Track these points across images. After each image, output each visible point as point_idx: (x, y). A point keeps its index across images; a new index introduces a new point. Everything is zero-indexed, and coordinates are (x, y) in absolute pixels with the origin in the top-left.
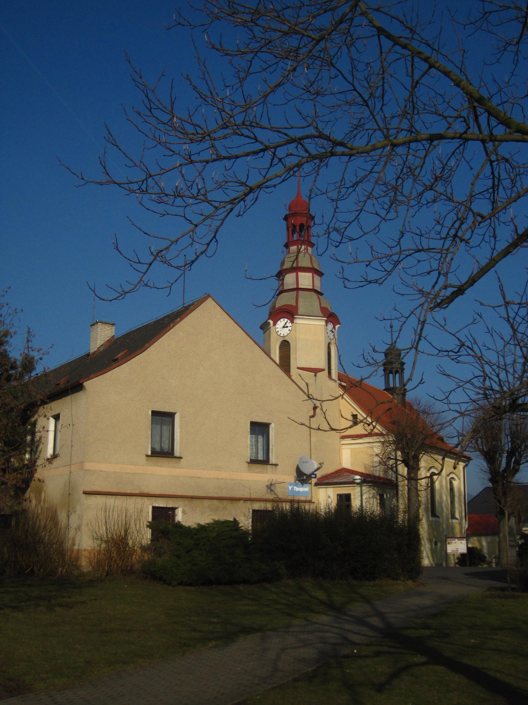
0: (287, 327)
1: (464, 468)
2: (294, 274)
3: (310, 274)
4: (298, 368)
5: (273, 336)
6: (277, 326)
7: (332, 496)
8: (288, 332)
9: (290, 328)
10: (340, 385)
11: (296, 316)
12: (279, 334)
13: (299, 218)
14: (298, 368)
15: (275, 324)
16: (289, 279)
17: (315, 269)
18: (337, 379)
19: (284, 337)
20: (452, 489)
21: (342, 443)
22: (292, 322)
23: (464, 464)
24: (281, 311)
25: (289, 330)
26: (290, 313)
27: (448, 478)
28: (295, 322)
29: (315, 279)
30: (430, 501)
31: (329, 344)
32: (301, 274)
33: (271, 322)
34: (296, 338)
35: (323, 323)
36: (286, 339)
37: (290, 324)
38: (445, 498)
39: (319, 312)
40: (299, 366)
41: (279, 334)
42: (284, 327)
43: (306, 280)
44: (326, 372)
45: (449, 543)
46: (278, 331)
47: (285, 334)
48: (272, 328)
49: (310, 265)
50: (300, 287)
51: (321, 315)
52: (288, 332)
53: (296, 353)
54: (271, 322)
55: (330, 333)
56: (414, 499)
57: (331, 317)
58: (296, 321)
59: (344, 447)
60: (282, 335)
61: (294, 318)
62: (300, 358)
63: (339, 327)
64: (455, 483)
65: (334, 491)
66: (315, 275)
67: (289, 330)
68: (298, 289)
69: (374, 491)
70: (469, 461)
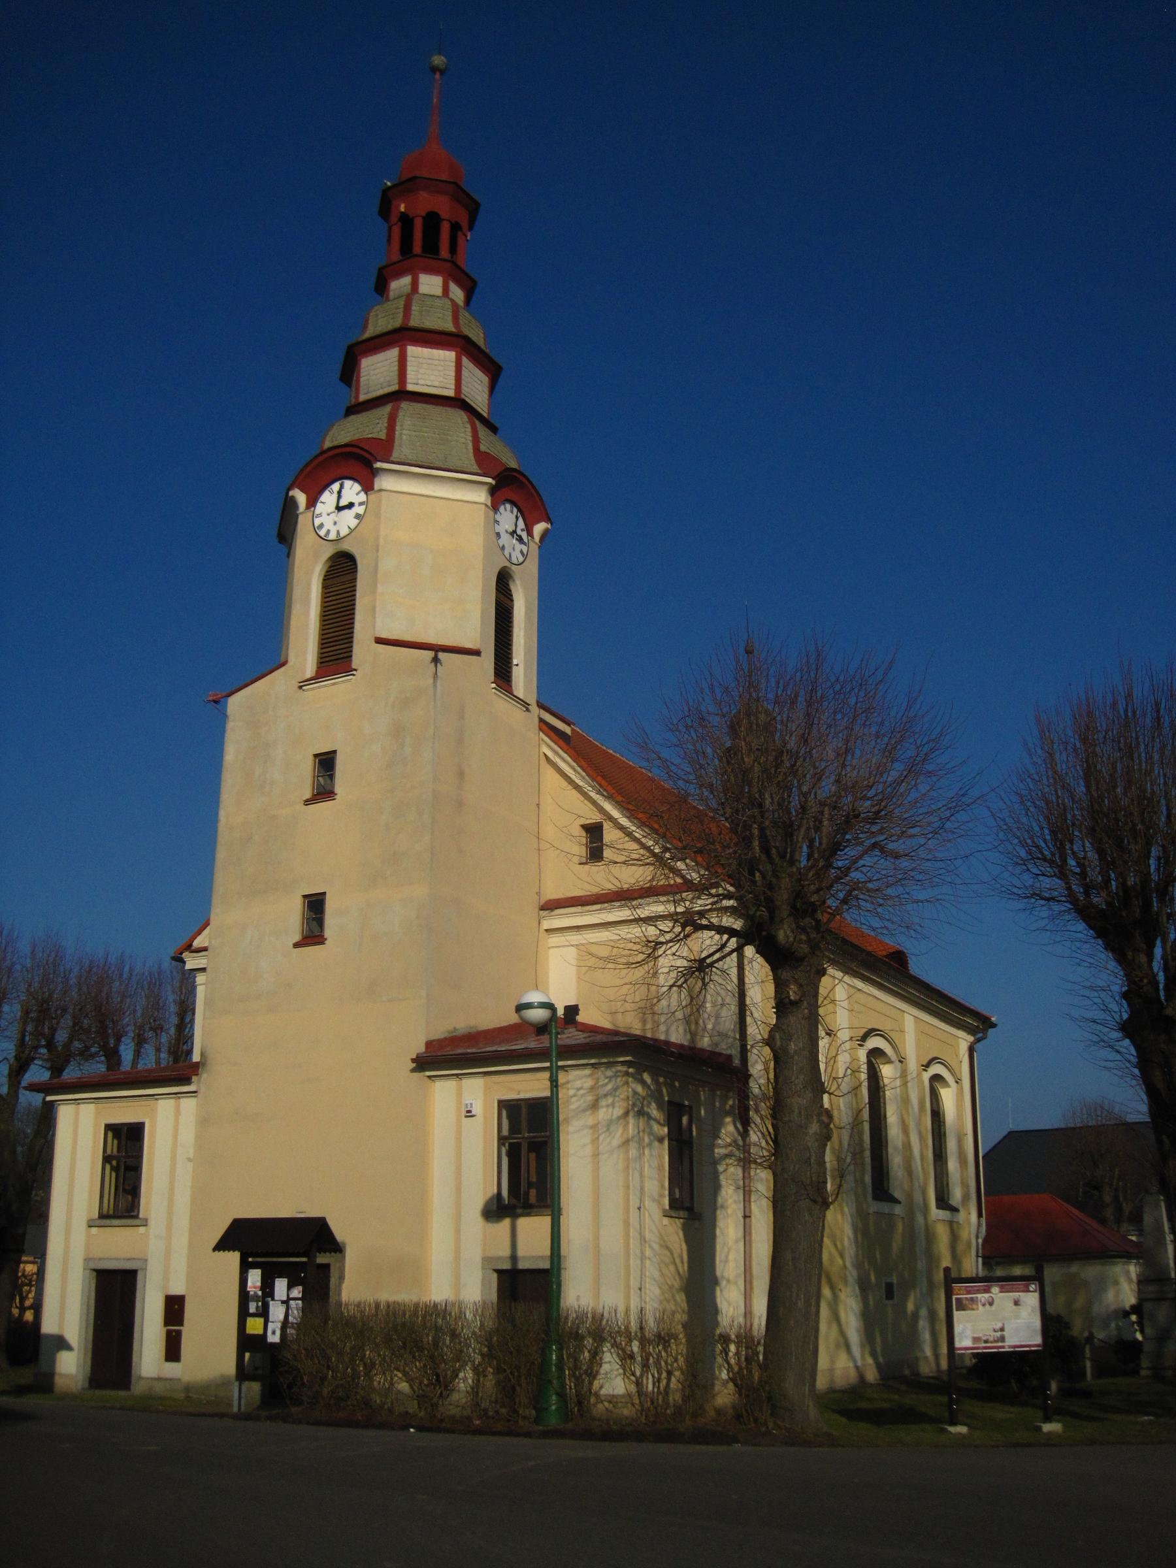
0: (350, 506)
1: (971, 1050)
2: (394, 353)
3: (449, 356)
4: (379, 641)
5: (304, 542)
6: (319, 508)
7: (477, 1109)
8: (353, 523)
9: (360, 510)
10: (544, 726)
11: (378, 465)
12: (322, 533)
13: (423, 195)
14: (379, 641)
15: (312, 503)
16: (377, 372)
17: (467, 339)
18: (532, 699)
19: (339, 540)
20: (937, 1115)
21: (546, 924)
22: (368, 487)
23: (971, 1038)
24: (332, 457)
25: (358, 516)
26: (360, 462)
27: (926, 1076)
28: (376, 487)
29: (465, 373)
30: (866, 1115)
31: (503, 581)
32: (412, 350)
33: (301, 498)
34: (377, 538)
35: (481, 496)
36: (346, 546)
37: (363, 497)
38: (921, 1148)
39: (470, 461)
40: (384, 635)
41: (317, 522)
42: (339, 509)
43: (432, 370)
44: (488, 661)
45: (961, 1307)
46: (321, 526)
47: (344, 532)
48: (303, 520)
49: (449, 327)
50: (410, 387)
51: (475, 468)
52: (353, 523)
53: (374, 591)
54: (301, 498)
55: (505, 540)
56: (798, 1102)
57: (509, 487)
58: (384, 482)
59: (555, 940)
60: (332, 536)
61: (374, 473)
62: (387, 607)
63: (545, 535)
64: (947, 1096)
65: (487, 1089)
66: (465, 361)
67: (358, 516)
68: (401, 395)
69: (639, 1089)
70: (985, 1031)
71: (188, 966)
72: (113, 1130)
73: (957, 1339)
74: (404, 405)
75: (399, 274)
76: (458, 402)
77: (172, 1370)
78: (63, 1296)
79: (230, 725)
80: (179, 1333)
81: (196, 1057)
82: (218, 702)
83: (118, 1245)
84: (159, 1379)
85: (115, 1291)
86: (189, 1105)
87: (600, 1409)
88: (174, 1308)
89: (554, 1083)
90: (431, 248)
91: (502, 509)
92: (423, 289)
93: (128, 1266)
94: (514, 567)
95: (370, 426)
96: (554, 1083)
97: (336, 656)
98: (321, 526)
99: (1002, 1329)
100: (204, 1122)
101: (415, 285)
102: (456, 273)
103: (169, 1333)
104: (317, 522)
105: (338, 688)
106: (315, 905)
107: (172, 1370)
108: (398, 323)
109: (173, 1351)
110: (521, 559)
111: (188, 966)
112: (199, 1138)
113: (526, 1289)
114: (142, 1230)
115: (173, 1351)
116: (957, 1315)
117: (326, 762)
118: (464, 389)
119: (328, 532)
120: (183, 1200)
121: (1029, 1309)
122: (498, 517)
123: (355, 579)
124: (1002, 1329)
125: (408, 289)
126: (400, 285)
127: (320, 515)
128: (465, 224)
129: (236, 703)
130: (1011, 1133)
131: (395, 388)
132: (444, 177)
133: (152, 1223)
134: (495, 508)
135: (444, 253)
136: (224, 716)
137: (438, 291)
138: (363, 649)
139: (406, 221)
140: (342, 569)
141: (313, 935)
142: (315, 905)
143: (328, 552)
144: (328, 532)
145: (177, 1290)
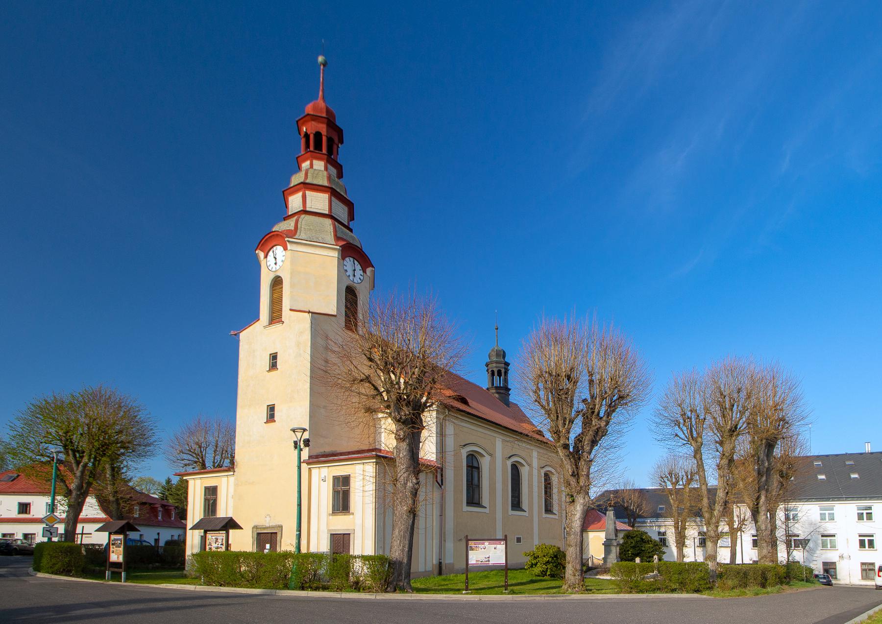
2: (300, 194)
4: (291, 310)
15: (266, 257)
16: (295, 202)
29: (333, 204)
54: (262, 255)
66: (333, 198)
68: (305, 212)
74: (303, 216)
75: (304, 161)
76: (330, 216)
79: (241, 344)
82: (237, 335)
86: (232, 479)
90: (318, 146)
95: (289, 225)
97: (275, 317)
100: (236, 485)
101: (311, 165)
102: (331, 160)
105: (277, 327)
106: (271, 409)
108: (302, 180)
112: (235, 491)
113: (340, 541)
118: (333, 211)
121: (568, 558)
122: (345, 263)
126: (306, 165)
128: (336, 141)
129: (243, 335)
130: (342, 131)
132: (324, 115)
134: (343, 258)
135: (324, 151)
136: (238, 341)
139: (307, 136)
140: (277, 282)
142: (271, 409)
143: (272, 276)
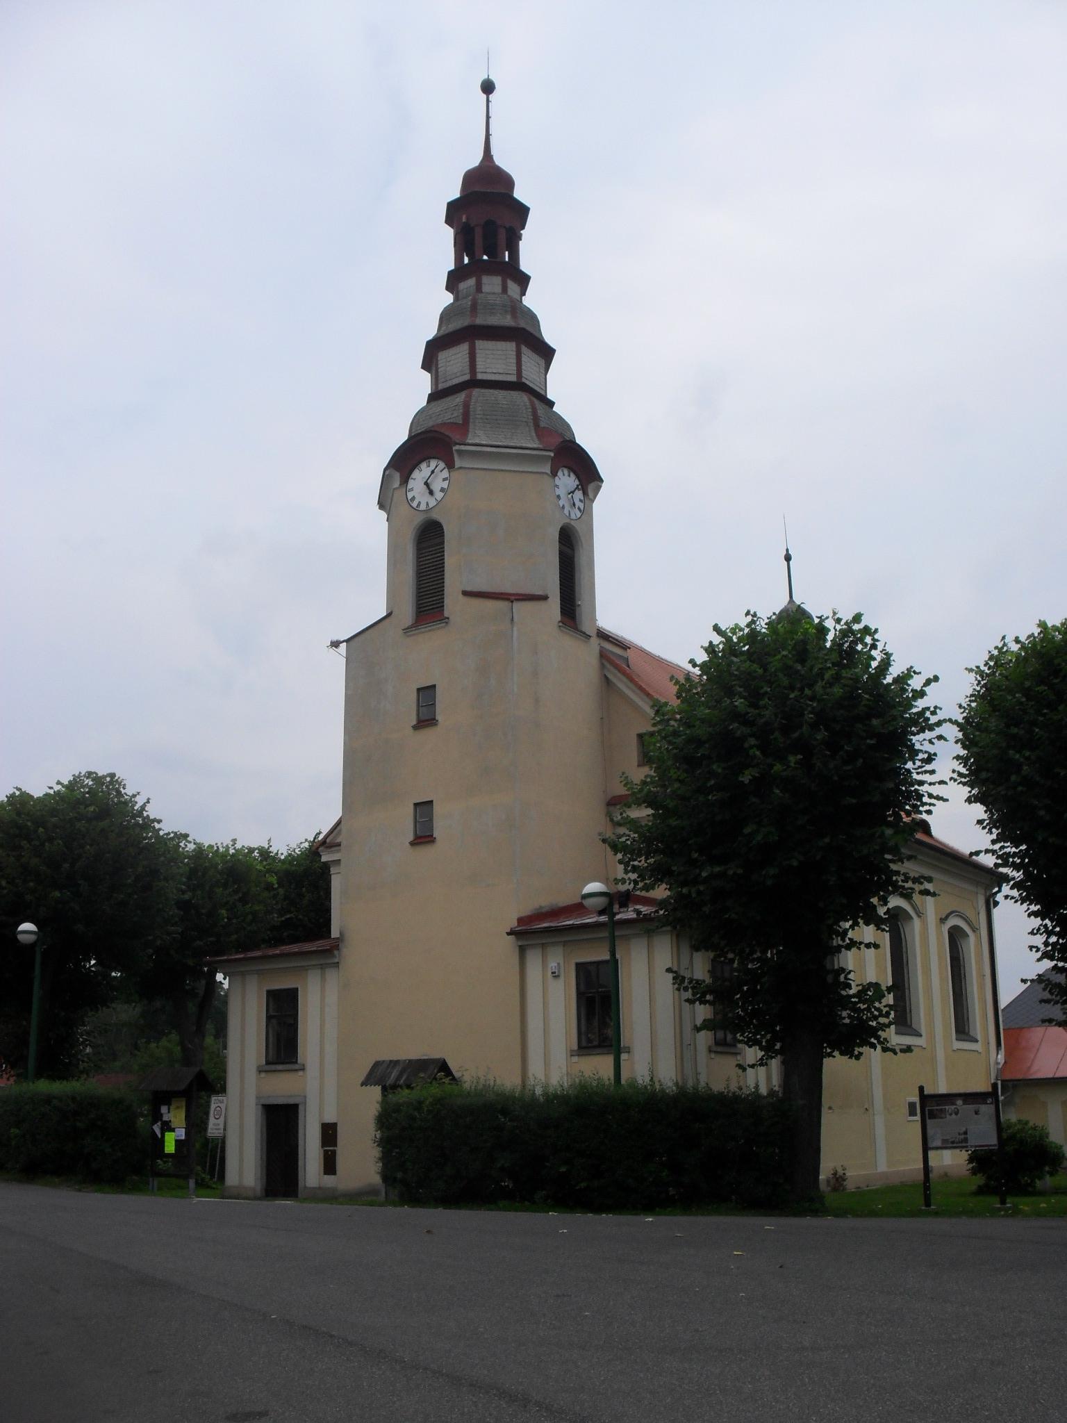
2: (464, 348)
3: (510, 347)
6: (411, 484)
19: (428, 510)
27: (945, 929)
29: (524, 359)
32: (480, 344)
36: (435, 516)
40: (469, 589)
41: (410, 495)
44: (554, 607)
46: (413, 498)
60: (423, 507)
66: (524, 349)
68: (474, 383)
71: (324, 859)
72: (272, 995)
73: (929, 1141)
77: (329, 1181)
78: (241, 1126)
80: (334, 1153)
81: (335, 933)
83: (281, 1087)
84: (320, 1188)
85: (281, 1122)
87: (467, 1086)
88: (329, 1133)
89: (613, 954)
91: (560, 473)
92: (486, 288)
93: (291, 1101)
94: (573, 523)
96: (613, 954)
98: (413, 498)
99: (965, 1133)
101: (479, 287)
103: (326, 1152)
104: (410, 495)
106: (424, 809)
107: (329, 1181)
109: (330, 1166)
110: (579, 514)
111: (324, 859)
114: (301, 1073)
115: (330, 1166)
116: (928, 1121)
117: (427, 694)
118: (524, 373)
119: (419, 504)
120: (331, 1049)
123: (443, 543)
124: (965, 1133)
125: (473, 290)
127: (412, 489)
131: (467, 377)
133: (308, 1067)
137: (498, 289)
138: (453, 602)
141: (423, 837)
142: (424, 809)
143: (419, 519)
144: (419, 504)
145: (329, 1119)
